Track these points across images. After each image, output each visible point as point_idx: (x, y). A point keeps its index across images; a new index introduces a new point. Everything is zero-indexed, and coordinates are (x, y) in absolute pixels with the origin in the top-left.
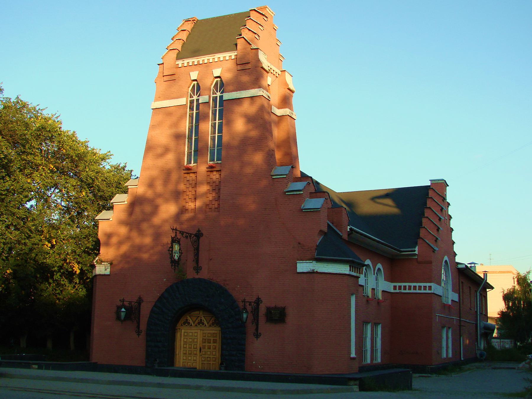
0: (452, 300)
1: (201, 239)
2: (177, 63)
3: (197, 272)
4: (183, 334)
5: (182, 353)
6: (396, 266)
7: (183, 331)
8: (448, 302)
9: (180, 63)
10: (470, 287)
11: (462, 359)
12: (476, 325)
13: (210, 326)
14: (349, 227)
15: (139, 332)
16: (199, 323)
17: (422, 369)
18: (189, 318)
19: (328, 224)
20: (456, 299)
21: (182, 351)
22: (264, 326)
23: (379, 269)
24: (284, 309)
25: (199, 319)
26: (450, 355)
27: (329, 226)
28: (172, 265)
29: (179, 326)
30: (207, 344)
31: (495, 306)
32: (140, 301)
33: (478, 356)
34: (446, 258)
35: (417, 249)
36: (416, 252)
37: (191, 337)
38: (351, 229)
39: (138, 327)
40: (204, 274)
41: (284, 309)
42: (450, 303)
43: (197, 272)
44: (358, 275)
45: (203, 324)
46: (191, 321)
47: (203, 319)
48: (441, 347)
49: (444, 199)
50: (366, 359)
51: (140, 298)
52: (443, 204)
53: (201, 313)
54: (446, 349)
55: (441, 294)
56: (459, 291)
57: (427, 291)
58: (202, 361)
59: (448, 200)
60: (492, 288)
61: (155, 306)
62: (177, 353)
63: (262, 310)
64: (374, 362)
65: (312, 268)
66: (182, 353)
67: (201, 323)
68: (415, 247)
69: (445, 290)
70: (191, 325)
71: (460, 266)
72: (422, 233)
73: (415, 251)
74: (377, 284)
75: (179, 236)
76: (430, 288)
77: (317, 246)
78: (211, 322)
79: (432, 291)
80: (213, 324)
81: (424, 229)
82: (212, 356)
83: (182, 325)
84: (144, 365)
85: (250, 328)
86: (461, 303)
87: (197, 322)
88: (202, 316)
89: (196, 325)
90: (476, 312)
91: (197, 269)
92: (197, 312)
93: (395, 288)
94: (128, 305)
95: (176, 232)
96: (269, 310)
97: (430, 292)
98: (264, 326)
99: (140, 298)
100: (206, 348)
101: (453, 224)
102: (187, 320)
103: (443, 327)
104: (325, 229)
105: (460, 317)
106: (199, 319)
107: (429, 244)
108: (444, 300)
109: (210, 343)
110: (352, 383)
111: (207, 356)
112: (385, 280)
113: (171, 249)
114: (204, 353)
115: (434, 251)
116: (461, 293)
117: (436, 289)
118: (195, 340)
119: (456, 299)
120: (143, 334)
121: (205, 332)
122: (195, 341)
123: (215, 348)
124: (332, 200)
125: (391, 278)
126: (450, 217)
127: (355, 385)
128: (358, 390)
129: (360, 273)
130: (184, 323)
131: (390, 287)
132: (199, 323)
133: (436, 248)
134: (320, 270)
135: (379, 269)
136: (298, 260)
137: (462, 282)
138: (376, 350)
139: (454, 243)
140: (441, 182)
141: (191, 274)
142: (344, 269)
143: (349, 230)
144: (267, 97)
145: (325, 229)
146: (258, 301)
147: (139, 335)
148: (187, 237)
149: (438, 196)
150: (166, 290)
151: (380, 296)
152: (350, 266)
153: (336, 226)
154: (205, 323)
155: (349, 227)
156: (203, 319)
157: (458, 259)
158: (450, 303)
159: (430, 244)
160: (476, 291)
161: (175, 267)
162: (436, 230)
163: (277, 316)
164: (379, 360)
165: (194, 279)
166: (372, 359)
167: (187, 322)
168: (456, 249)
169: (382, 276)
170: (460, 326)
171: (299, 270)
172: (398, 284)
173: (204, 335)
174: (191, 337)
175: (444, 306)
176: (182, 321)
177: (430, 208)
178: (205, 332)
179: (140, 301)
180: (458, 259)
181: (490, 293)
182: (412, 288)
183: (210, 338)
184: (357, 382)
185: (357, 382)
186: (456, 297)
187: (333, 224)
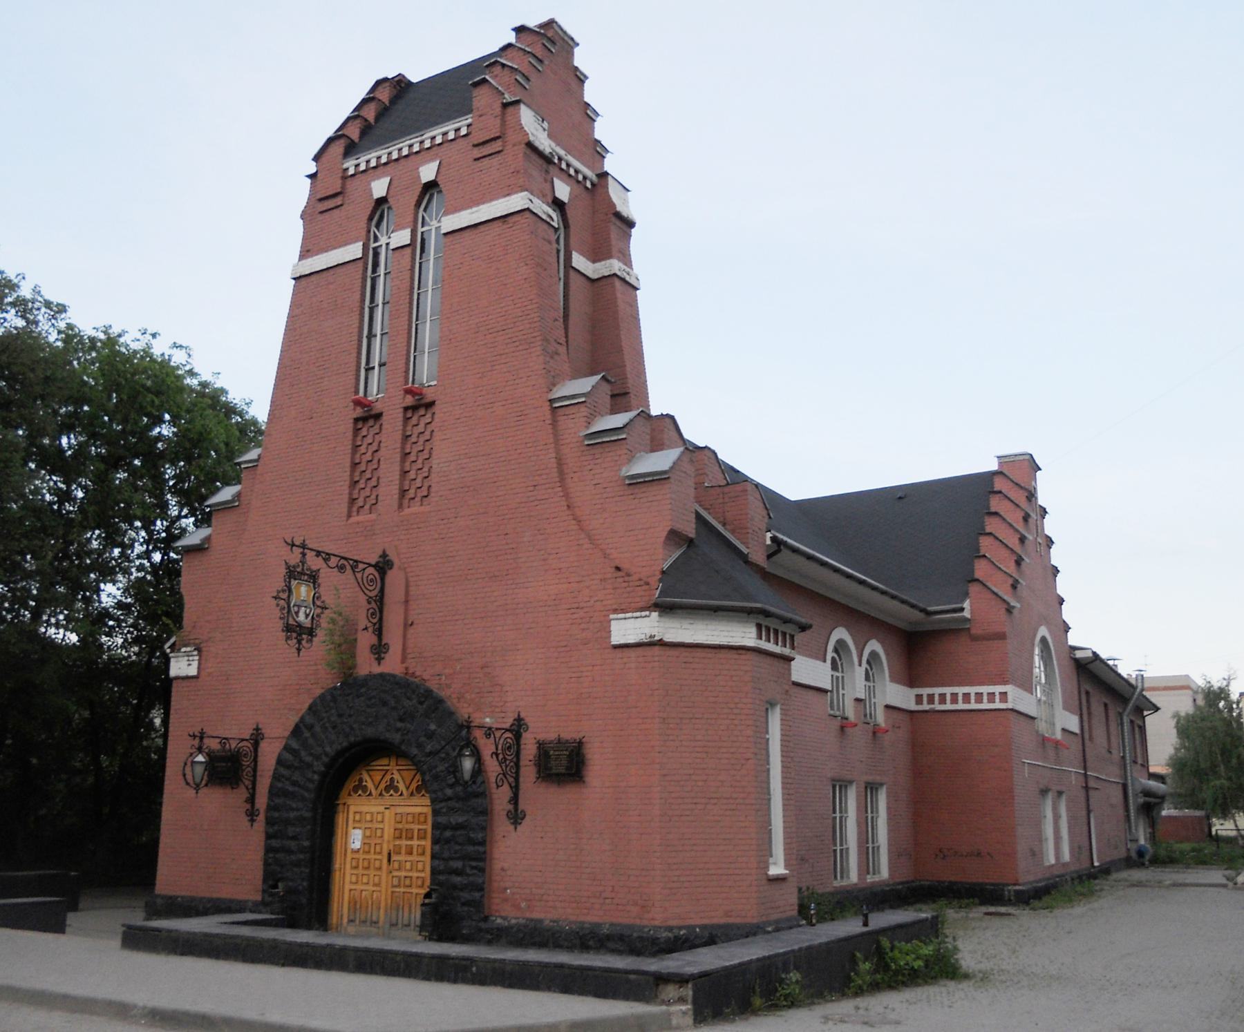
0: (1063, 730)
1: (391, 576)
2: (345, 166)
3: (379, 660)
4: (351, 816)
5: (348, 866)
6: (919, 648)
7: (352, 809)
8: (1054, 734)
9: (350, 165)
10: (1106, 705)
11: (1096, 864)
12: (1125, 787)
13: (412, 794)
14: (769, 535)
15: (252, 815)
16: (387, 789)
17: (989, 896)
18: (365, 776)
19: (697, 513)
20: (1075, 728)
21: (349, 859)
22: (534, 792)
23: (874, 654)
24: (580, 743)
25: (388, 777)
26: (1066, 856)
27: (699, 517)
28: (288, 638)
29: (343, 797)
30: (404, 842)
31: (1162, 743)
32: (257, 737)
33: (1134, 855)
34: (1043, 631)
35: (966, 605)
36: (967, 614)
37: (369, 825)
38: (774, 539)
39: (251, 800)
40: (392, 665)
41: (580, 743)
42: (1059, 735)
43: (379, 660)
44: (787, 651)
45: (396, 789)
46: (370, 785)
47: (397, 776)
48: (1040, 839)
49: (1031, 496)
50: (845, 872)
51: (257, 729)
52: (1033, 513)
53: (393, 762)
54: (1053, 840)
55: (1033, 713)
56: (1081, 709)
57: (998, 705)
58: (394, 886)
59: (1042, 500)
60: (1157, 709)
61: (287, 748)
62: (337, 866)
63: (529, 750)
64: (870, 879)
65: (649, 632)
66: (348, 866)
67: (391, 786)
68: (963, 601)
69: (1043, 703)
70: (370, 794)
71: (1079, 654)
72: (981, 569)
73: (962, 609)
74: (871, 691)
75: (314, 562)
76: (1004, 696)
77: (663, 572)
78: (414, 785)
79: (1010, 705)
80: (418, 789)
81: (983, 562)
82: (415, 874)
83: (349, 795)
84: (259, 898)
85: (500, 798)
86: (1087, 736)
87: (383, 786)
88: (398, 772)
89: (381, 794)
90: (1123, 758)
91: (379, 650)
92: (385, 761)
93: (919, 699)
94: (219, 747)
95: (304, 555)
96: (544, 752)
97: (1003, 706)
98: (534, 792)
99: (257, 729)
100: (403, 851)
101: (1050, 526)
102: (361, 780)
103: (1044, 792)
104: (690, 529)
105: (1085, 768)
106: (388, 777)
107: (996, 594)
108: (1042, 727)
109: (412, 838)
110: (671, 991)
111: (403, 874)
112: (894, 679)
113: (285, 596)
114: (396, 865)
115: (1009, 610)
116: (1085, 717)
117: (1018, 699)
118: (379, 834)
119: (1075, 728)
120: (261, 818)
121: (399, 810)
122: (381, 837)
123: (423, 854)
124: (905, 632)
125: (911, 676)
126: (1050, 542)
127: (682, 1000)
128: (689, 1020)
129: (793, 648)
130: (356, 789)
131: (898, 695)
132: (387, 789)
133: (1013, 603)
134: (670, 637)
135: (874, 654)
136: (615, 611)
137: (1087, 693)
138: (876, 849)
139: (1061, 601)
140: (1021, 458)
141: (366, 666)
142: (744, 635)
143: (768, 542)
144: (544, 217)
145: (690, 529)
146: (518, 728)
147: (252, 821)
148: (341, 568)
149: (1016, 488)
150: (310, 708)
151: (881, 718)
152: (759, 627)
153: (733, 532)
154: (401, 786)
155: (769, 535)
156: (397, 776)
157: (1073, 639)
158: (1059, 735)
159: (1000, 593)
160: (1121, 715)
161: (299, 642)
162: (1013, 564)
163: (565, 764)
164: (885, 873)
165: (372, 676)
166: (865, 868)
167: (360, 787)
168: (1068, 613)
169: (883, 671)
170: (1087, 788)
171: (616, 639)
172: (925, 691)
173: (398, 819)
174: (369, 825)
175: (1044, 741)
176: (350, 784)
177: (996, 514)
178: (399, 810)
179: (257, 737)
180: (1073, 639)
181: (1151, 721)
182: (960, 698)
183: (412, 826)
184: (688, 992)
185: (688, 992)
186: (1073, 723)
187: (724, 525)
